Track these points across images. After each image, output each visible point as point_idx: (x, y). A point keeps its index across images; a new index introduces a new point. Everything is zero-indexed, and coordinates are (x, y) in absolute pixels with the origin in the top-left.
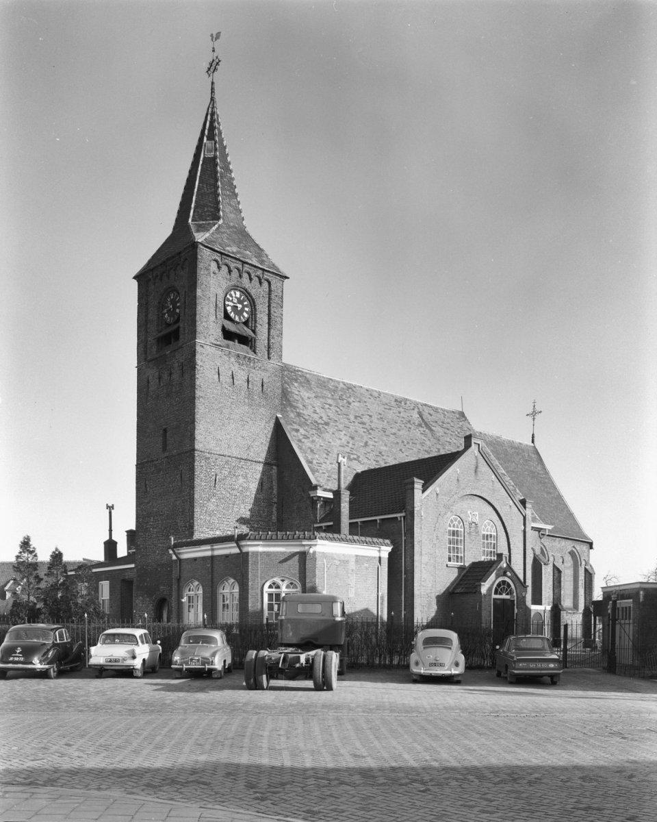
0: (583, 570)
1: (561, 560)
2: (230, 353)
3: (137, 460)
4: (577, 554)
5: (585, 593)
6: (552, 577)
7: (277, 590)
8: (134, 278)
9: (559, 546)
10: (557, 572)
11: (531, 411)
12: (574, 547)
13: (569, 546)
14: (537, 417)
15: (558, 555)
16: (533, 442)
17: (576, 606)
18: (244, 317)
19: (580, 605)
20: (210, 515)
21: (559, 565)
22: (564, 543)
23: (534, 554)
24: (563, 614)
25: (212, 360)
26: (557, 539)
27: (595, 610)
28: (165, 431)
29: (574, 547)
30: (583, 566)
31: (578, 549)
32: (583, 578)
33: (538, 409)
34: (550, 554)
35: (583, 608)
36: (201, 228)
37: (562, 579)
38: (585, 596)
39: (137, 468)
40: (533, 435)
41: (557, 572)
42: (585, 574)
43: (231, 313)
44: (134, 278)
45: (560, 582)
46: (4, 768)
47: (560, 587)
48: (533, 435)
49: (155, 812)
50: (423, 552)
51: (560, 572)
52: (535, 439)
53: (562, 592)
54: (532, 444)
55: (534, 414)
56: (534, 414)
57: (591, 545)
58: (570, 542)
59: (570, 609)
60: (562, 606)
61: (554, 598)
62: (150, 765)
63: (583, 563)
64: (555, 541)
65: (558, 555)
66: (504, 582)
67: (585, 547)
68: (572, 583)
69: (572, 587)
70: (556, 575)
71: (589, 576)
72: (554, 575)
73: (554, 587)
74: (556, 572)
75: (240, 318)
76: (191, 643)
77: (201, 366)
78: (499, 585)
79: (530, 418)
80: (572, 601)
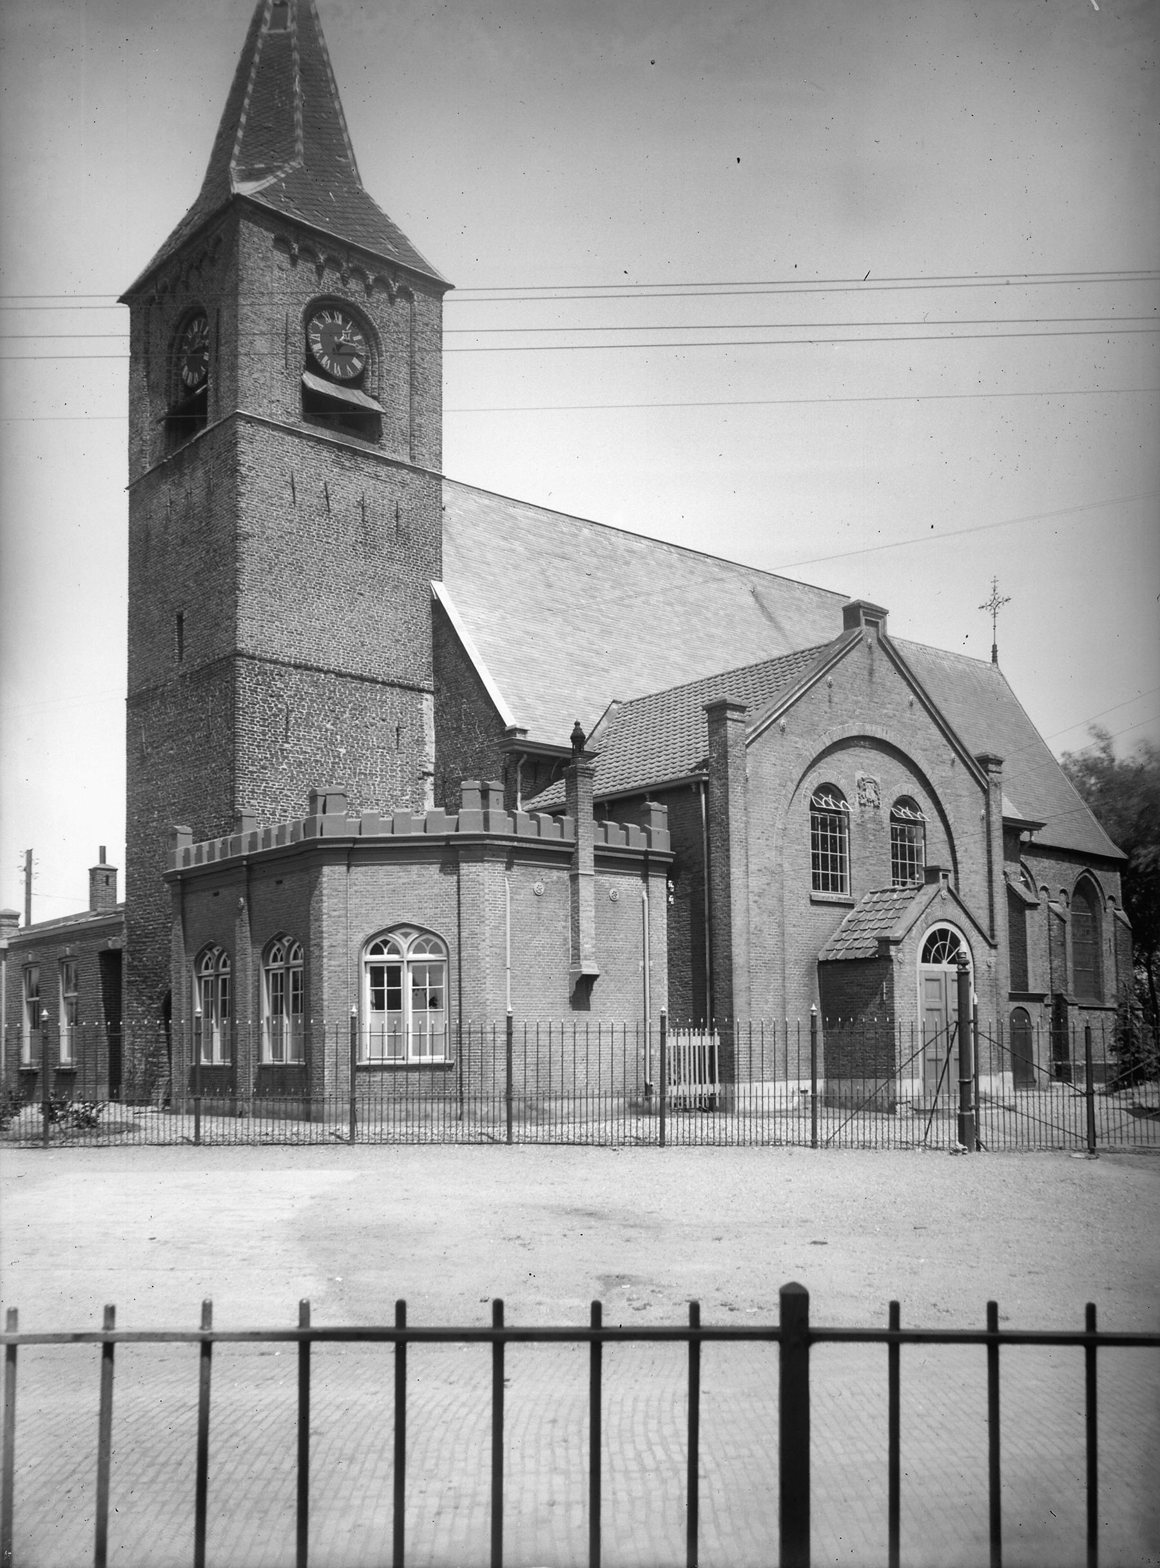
3: (129, 690)
7: (395, 957)
8: (123, 300)
11: (987, 598)
16: (995, 659)
18: (353, 367)
20: (275, 800)
25: (276, 471)
28: (180, 618)
33: (1002, 594)
36: (249, 175)
39: (129, 707)
40: (994, 647)
43: (322, 356)
44: (123, 300)
46: (287, 1215)
48: (994, 647)
50: (752, 867)
55: (994, 605)
62: (906, 1029)
66: (943, 933)
75: (343, 369)
76: (705, 1021)
77: (250, 469)
78: (932, 940)
79: (987, 614)
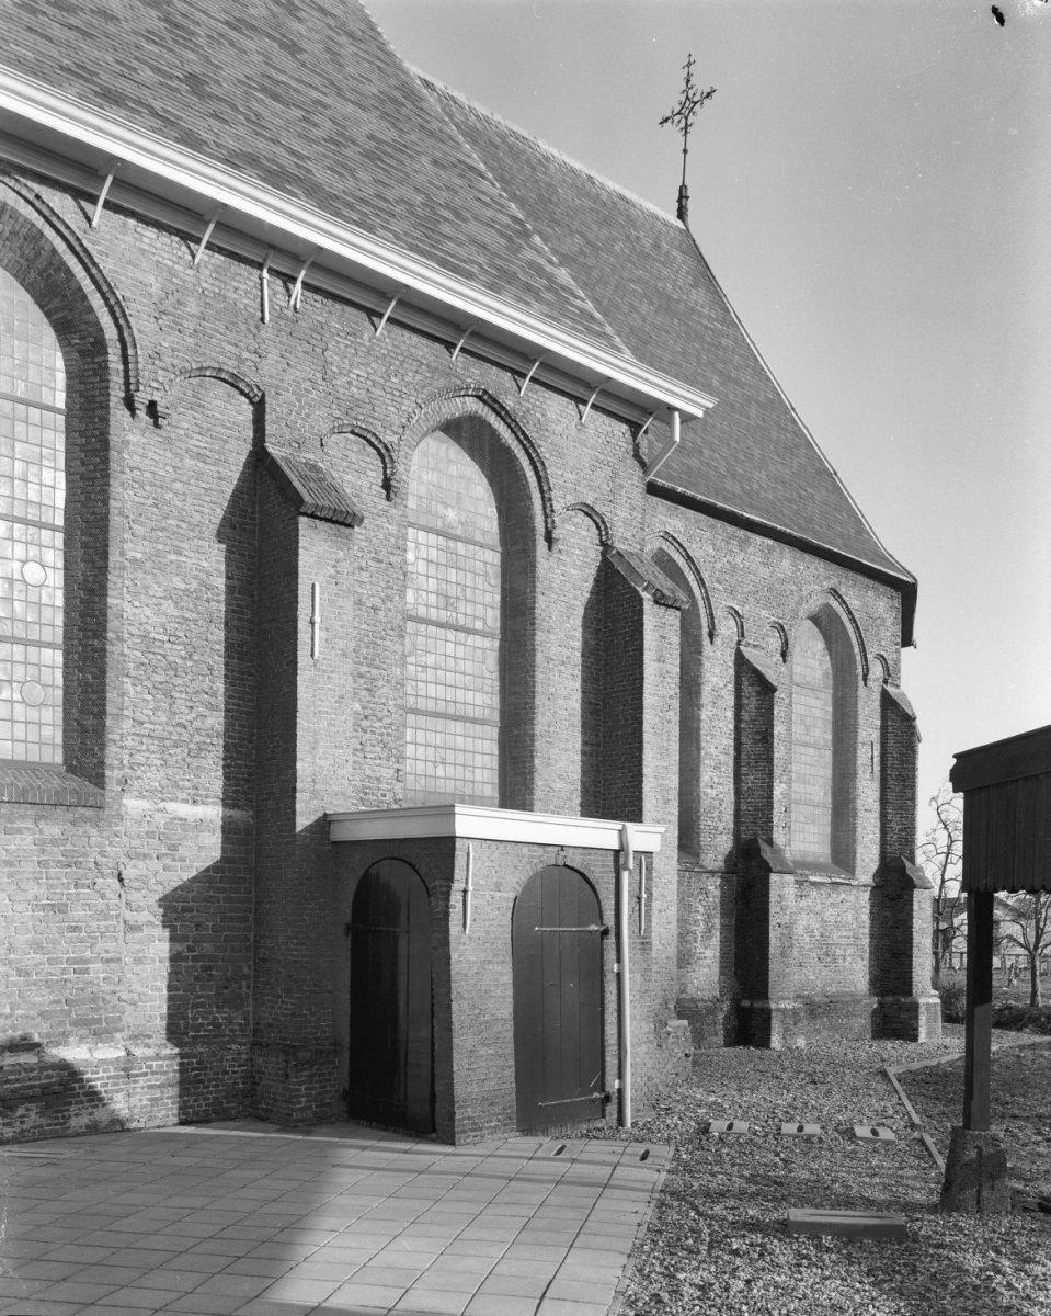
0: (877, 696)
1: (775, 643)
2: (598, 680)
4: (845, 618)
5: (883, 801)
6: (730, 714)
9: (764, 572)
10: (755, 688)
12: (834, 592)
13: (811, 581)
14: (700, 118)
15: (760, 616)
17: (842, 854)
19: (860, 850)
21: (765, 659)
22: (787, 562)
23: (606, 546)
24: (782, 888)
26: (758, 539)
27: (71, 769)
29: (834, 592)
30: (875, 686)
31: (854, 603)
32: (876, 736)
33: (701, 84)
34: (721, 604)
35: (874, 866)
37: (779, 729)
38: (883, 815)
40: (683, 189)
41: (755, 688)
42: (884, 718)
45: (766, 738)
47: (770, 760)
48: (683, 189)
49: (217, 1176)
51: (766, 689)
52: (691, 205)
53: (779, 790)
54: (679, 223)
55: (684, 113)
56: (684, 113)
57: (907, 593)
58: (817, 566)
59: (816, 867)
60: (778, 852)
61: (737, 814)
63: (877, 671)
64: (743, 544)
65: (760, 616)
67: (879, 607)
68: (828, 755)
69: (829, 772)
70: (751, 703)
71: (899, 726)
72: (738, 707)
73: (737, 760)
74: (747, 689)
79: (672, 130)
80: (828, 830)
